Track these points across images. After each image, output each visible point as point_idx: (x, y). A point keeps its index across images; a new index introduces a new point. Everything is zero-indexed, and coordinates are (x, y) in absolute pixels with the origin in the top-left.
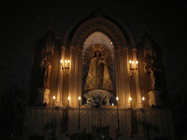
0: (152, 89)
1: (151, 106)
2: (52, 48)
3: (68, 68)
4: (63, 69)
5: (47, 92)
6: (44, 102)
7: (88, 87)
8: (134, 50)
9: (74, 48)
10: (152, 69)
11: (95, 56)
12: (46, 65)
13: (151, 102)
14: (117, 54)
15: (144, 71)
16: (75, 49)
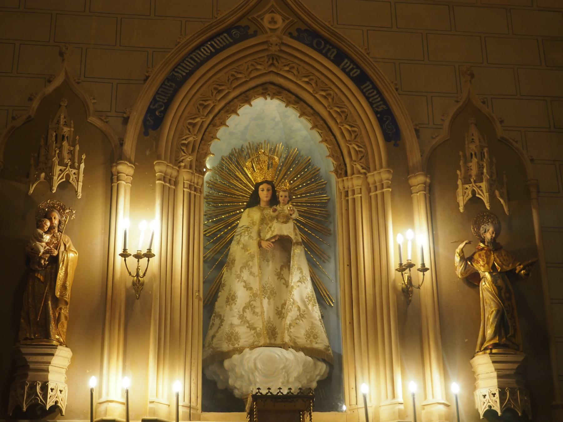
0: (486, 345)
1: (482, 413)
2: (79, 168)
3: (149, 255)
4: (125, 255)
5: (62, 357)
6: (50, 403)
7: (232, 337)
8: (418, 180)
9: (169, 171)
10: (488, 263)
11: (254, 201)
12: (57, 247)
13: (485, 396)
14: (347, 195)
15: (455, 269)
16: (175, 173)
